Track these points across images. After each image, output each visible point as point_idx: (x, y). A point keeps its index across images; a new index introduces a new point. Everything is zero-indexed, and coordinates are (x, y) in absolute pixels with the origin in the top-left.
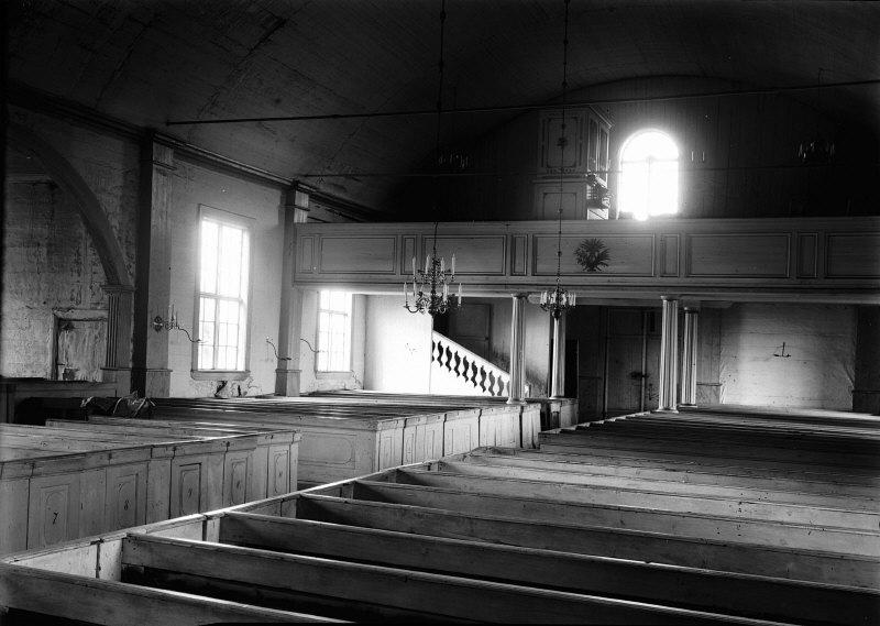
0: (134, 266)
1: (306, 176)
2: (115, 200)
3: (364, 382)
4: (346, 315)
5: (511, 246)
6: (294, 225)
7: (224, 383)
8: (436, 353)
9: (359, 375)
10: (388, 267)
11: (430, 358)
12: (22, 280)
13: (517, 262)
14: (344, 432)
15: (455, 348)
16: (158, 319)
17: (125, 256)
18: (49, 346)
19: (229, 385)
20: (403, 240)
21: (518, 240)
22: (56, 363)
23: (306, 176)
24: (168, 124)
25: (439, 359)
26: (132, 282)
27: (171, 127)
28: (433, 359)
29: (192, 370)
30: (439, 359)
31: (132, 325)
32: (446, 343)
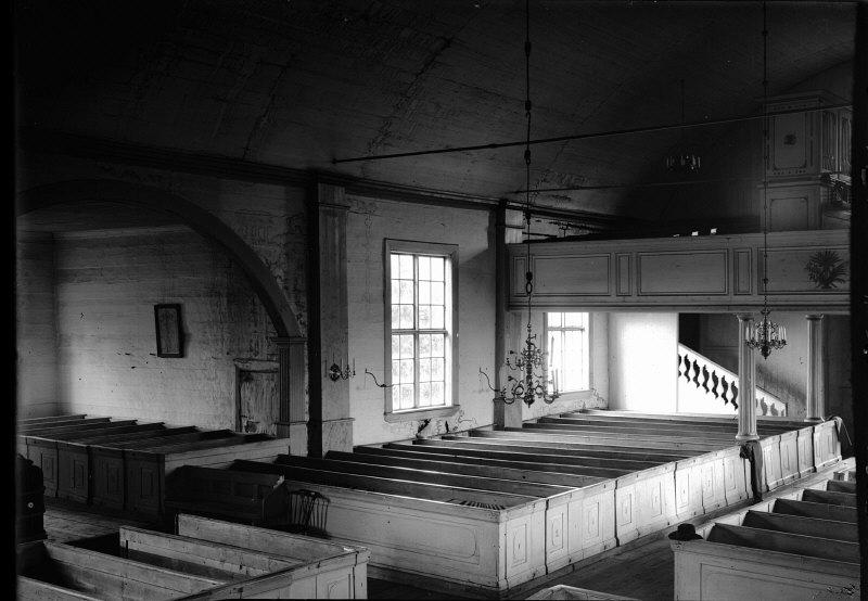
0: (305, 314)
1: (517, 192)
2: (278, 249)
3: (609, 399)
4: (582, 330)
5: (733, 261)
6: (506, 245)
7: (427, 422)
8: (683, 368)
9: (601, 390)
10: (602, 289)
11: (676, 374)
12: (207, 330)
13: (741, 280)
14: (467, 521)
15: (702, 362)
16: (335, 368)
17: (293, 307)
18: (233, 397)
19: (433, 424)
20: (618, 261)
21: (743, 257)
22: (239, 416)
23: (517, 192)
24: (335, 161)
25: (686, 374)
26: (303, 331)
27: (338, 164)
28: (680, 374)
29: (385, 414)
30: (686, 374)
31: (307, 376)
32: (693, 356)
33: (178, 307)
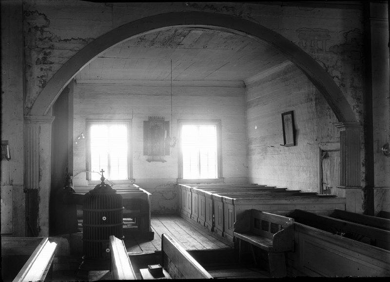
22: (322, 184)
33: (292, 113)
